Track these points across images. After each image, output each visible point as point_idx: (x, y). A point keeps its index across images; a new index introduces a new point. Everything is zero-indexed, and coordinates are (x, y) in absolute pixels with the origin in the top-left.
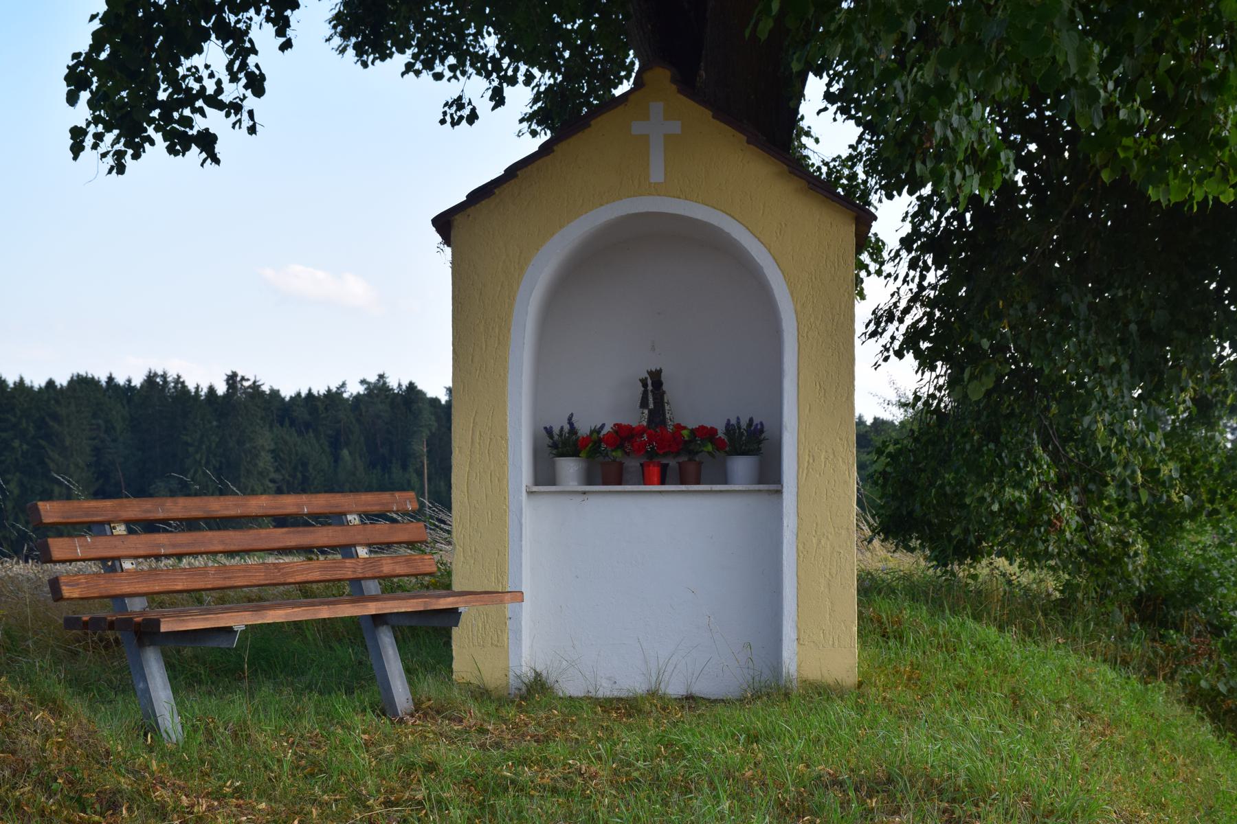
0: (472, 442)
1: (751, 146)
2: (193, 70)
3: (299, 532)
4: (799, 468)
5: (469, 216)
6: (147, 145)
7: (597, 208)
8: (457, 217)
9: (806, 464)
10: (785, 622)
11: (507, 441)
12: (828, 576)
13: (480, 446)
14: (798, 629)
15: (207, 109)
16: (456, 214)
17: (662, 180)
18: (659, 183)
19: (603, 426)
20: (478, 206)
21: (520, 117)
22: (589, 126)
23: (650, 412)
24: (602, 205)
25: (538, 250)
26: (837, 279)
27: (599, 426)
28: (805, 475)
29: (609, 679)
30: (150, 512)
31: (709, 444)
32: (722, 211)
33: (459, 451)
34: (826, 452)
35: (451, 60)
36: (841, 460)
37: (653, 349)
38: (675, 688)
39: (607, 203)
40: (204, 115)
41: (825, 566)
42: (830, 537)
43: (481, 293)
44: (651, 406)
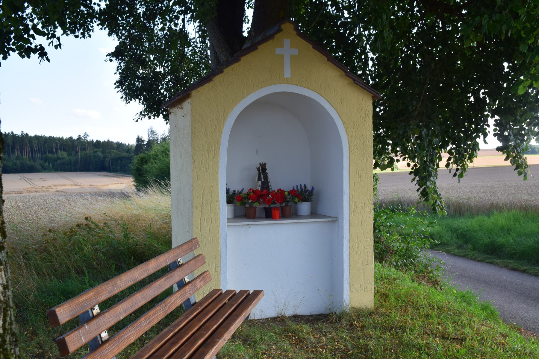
0: (202, 204)
1: (329, 62)
2: (29, 15)
3: (168, 278)
4: (350, 212)
5: (199, 91)
6: (11, 52)
7: (260, 89)
8: (193, 92)
9: (353, 209)
10: (344, 282)
11: (219, 202)
12: (362, 259)
13: (206, 205)
14: (350, 284)
15: (36, 36)
16: (193, 90)
17: (289, 76)
18: (288, 78)
19: (243, 190)
20: (203, 86)
21: (107, 54)
22: (257, 49)
23: (262, 183)
24: (262, 88)
25: (233, 109)
26: (365, 125)
27: (241, 190)
28: (352, 214)
29: (260, 310)
30: (112, 291)
31: (296, 198)
32: (316, 92)
33: (196, 209)
34: (361, 204)
35: (81, 31)
36: (367, 207)
37: (257, 153)
38: (289, 313)
39: (265, 87)
40: (34, 38)
41: (361, 255)
42: (363, 242)
43: (205, 130)
44: (263, 180)
